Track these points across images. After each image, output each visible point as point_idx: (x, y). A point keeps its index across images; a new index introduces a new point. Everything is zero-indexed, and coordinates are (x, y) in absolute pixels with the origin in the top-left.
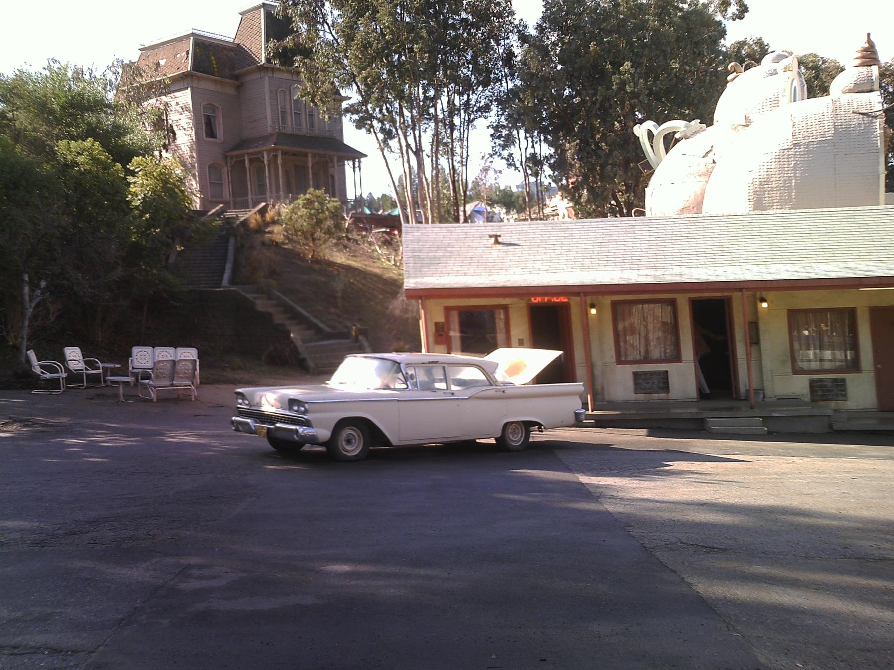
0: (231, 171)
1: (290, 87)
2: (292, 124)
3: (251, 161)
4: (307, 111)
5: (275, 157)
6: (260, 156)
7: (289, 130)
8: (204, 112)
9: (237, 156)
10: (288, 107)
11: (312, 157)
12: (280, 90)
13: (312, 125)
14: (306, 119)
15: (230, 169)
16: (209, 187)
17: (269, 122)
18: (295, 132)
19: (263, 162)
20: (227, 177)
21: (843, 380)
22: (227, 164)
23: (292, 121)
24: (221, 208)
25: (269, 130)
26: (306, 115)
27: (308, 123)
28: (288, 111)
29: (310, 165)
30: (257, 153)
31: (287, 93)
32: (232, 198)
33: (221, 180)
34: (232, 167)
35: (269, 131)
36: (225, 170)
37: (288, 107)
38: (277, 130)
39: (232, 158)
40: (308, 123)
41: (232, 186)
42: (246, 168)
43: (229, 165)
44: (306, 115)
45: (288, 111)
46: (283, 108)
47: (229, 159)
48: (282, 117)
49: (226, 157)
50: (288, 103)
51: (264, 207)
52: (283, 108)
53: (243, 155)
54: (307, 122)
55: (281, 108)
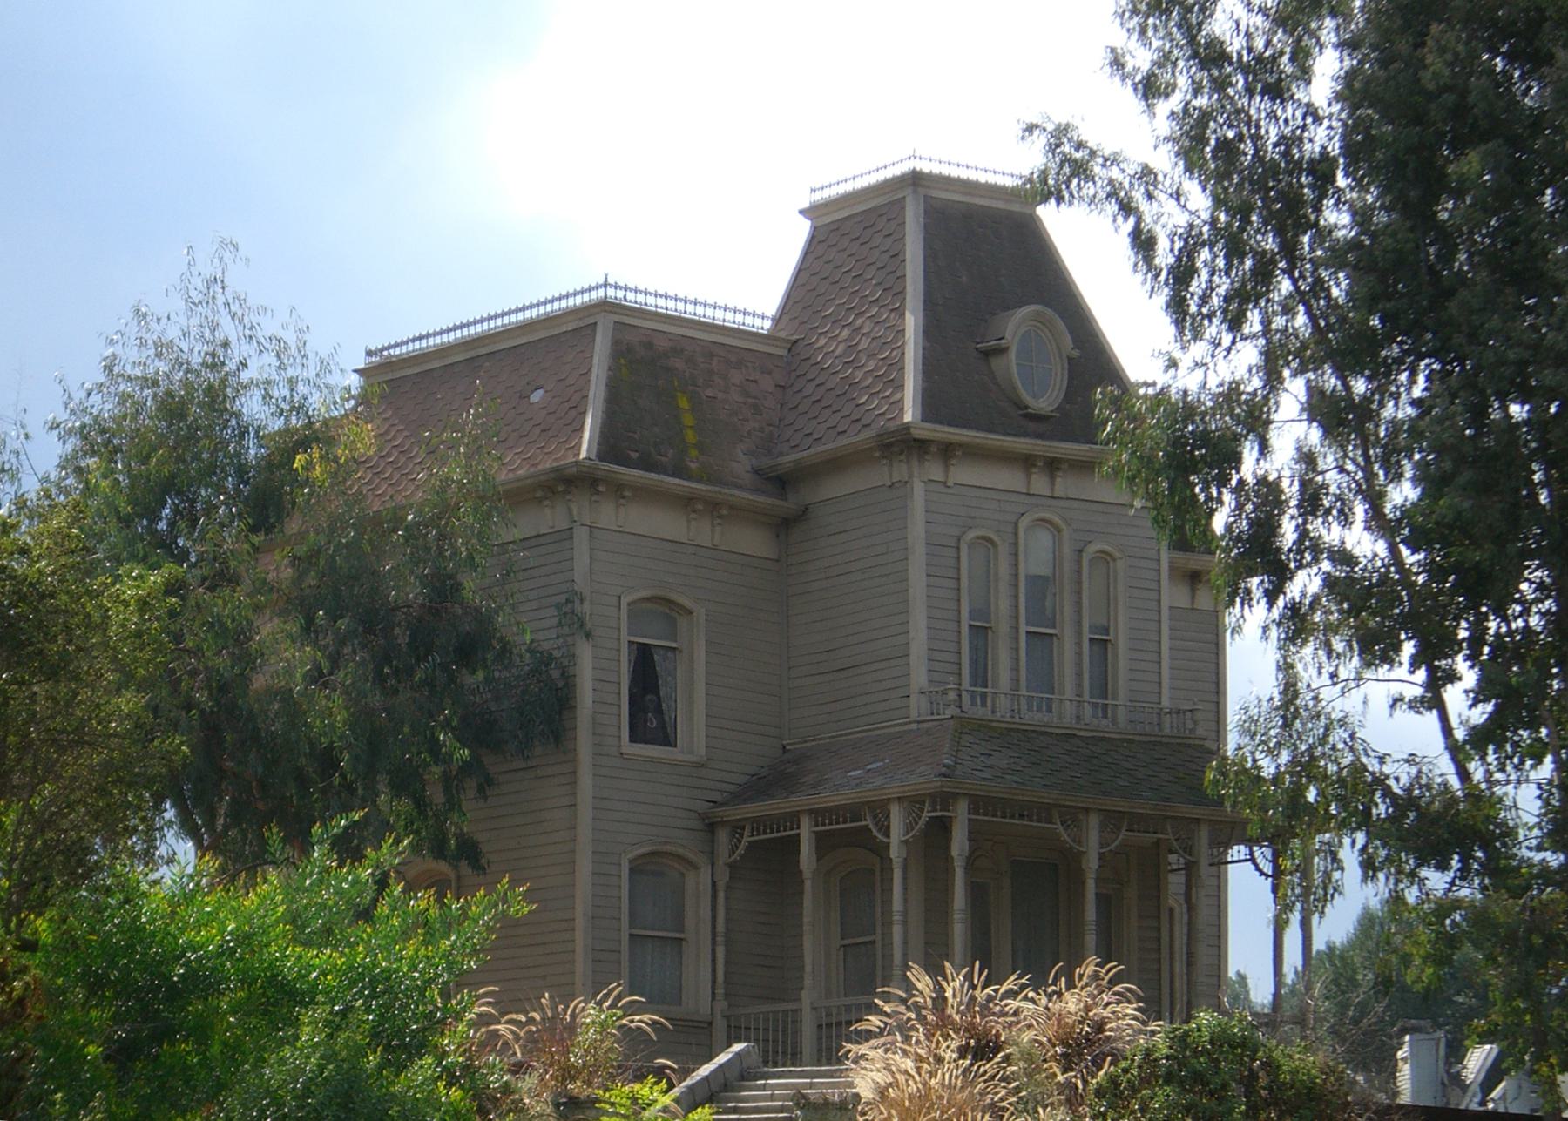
0: (728, 888)
1: (1016, 524)
2: (1016, 681)
3: (824, 843)
4: (1086, 628)
5: (941, 827)
6: (869, 822)
7: (1001, 709)
8: (629, 634)
9: (759, 824)
10: (1003, 605)
11: (1103, 827)
12: (971, 535)
13: (1103, 686)
14: (1079, 664)
15: (723, 877)
16: (625, 956)
17: (919, 677)
18: (1033, 718)
19: (882, 851)
20: (706, 912)
21: (1027, 576)
22: (712, 855)
23: (1015, 668)
24: (738, 1054)
25: (918, 707)
26: (1079, 644)
27: (1086, 676)
28: (1004, 628)
29: (1091, 863)
30: (854, 812)
31: (1004, 550)
32: (721, 1004)
33: (682, 929)
34: (732, 866)
35: (914, 715)
36: (699, 883)
37: (1003, 605)
38: (951, 711)
39: (737, 828)
40: (1086, 676)
41: (727, 952)
42: (948, 859)
43: (720, 862)
44: (1079, 644)
45: (1004, 628)
46: (982, 612)
47: (722, 836)
48: (974, 649)
49: (711, 828)
50: (1004, 589)
51: (1492, 1090)
52: (982, 612)
53: (793, 819)
54: (1079, 675)
55: (972, 616)
